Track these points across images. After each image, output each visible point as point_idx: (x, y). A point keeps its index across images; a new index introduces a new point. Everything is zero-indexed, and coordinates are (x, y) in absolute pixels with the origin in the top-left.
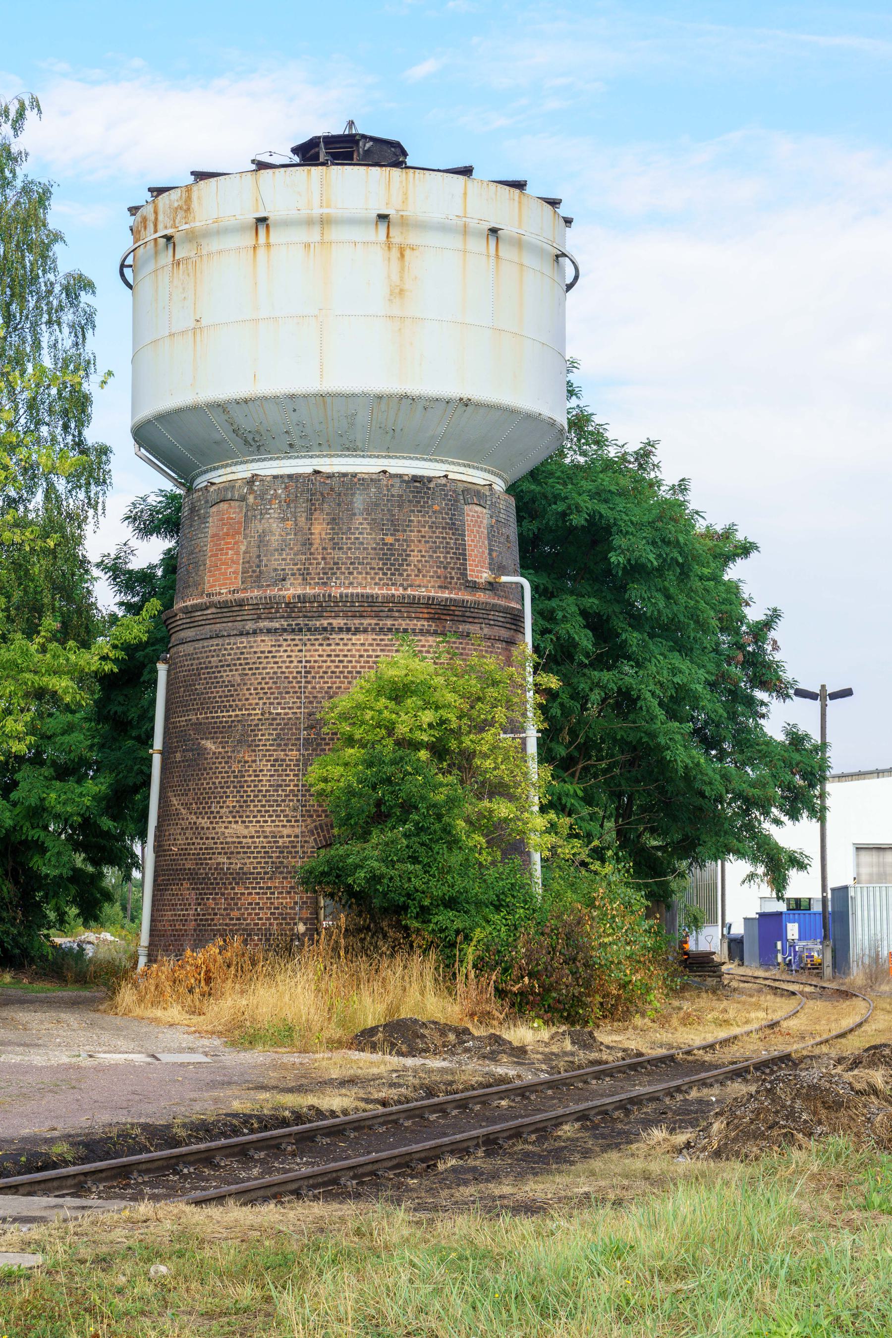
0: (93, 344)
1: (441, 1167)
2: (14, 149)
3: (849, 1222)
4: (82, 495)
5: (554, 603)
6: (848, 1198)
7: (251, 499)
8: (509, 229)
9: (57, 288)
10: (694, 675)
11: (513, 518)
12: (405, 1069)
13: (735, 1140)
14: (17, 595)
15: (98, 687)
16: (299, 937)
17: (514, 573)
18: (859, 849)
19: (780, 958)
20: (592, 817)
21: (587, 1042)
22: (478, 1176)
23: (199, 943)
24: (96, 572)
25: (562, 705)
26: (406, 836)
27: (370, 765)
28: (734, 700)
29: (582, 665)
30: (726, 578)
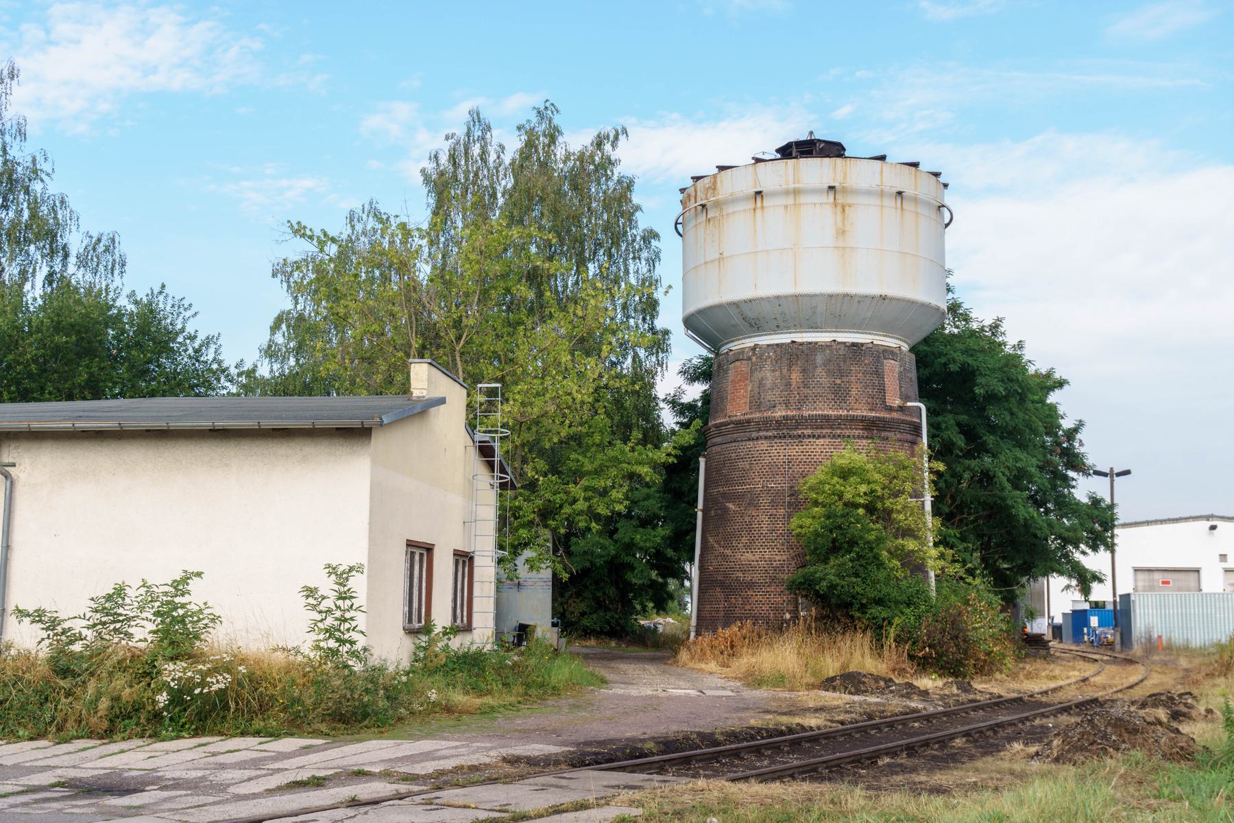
0: (660, 270)
1: (880, 763)
2: (613, 158)
3: (1149, 806)
4: (654, 359)
5: (940, 419)
6: (1146, 790)
7: (754, 359)
8: (909, 191)
9: (638, 238)
10: (1030, 462)
11: (914, 367)
12: (854, 702)
13: (1068, 751)
14: (617, 418)
15: (664, 472)
16: (787, 622)
17: (915, 401)
18: (1136, 570)
19: (1086, 638)
20: (966, 549)
21: (967, 688)
22: (904, 769)
23: (727, 624)
24: (662, 405)
25: (946, 481)
26: (851, 560)
27: (828, 517)
28: (1055, 477)
29: (957, 456)
30: (1048, 401)
